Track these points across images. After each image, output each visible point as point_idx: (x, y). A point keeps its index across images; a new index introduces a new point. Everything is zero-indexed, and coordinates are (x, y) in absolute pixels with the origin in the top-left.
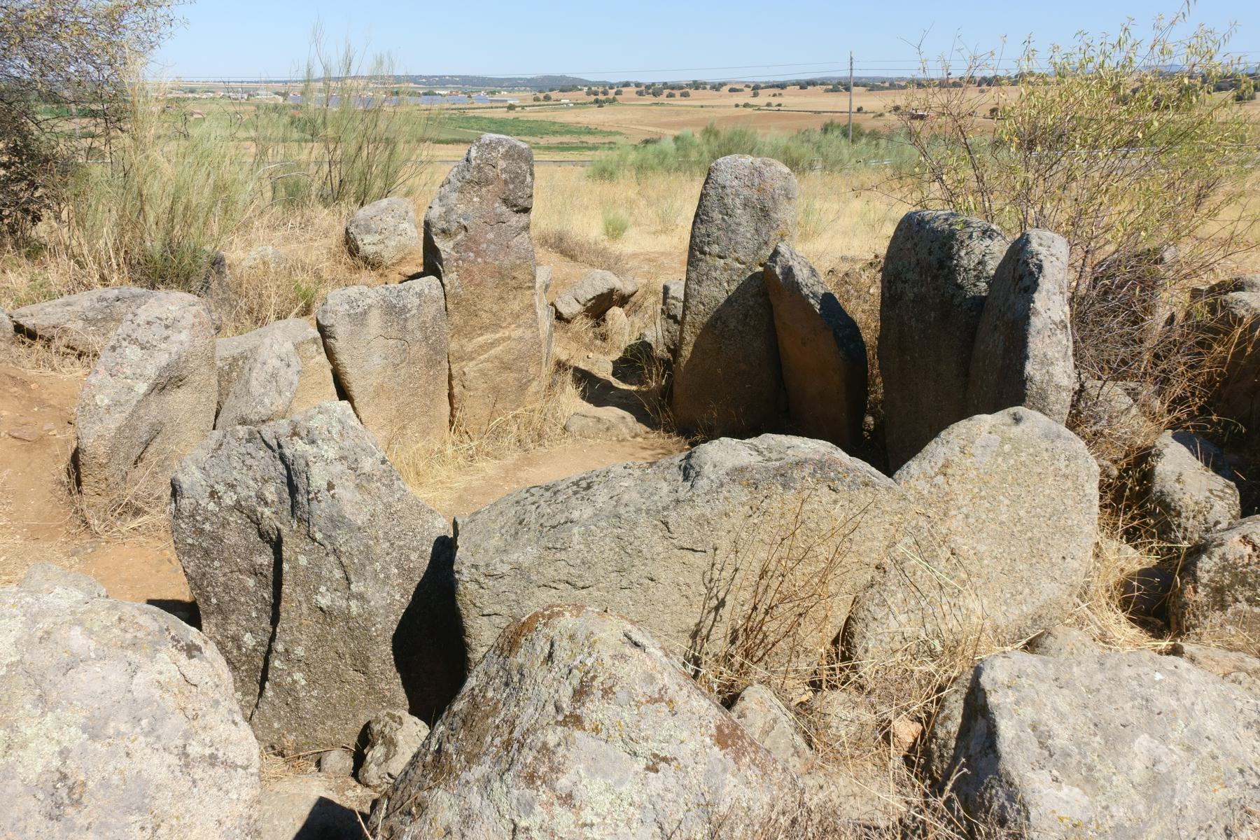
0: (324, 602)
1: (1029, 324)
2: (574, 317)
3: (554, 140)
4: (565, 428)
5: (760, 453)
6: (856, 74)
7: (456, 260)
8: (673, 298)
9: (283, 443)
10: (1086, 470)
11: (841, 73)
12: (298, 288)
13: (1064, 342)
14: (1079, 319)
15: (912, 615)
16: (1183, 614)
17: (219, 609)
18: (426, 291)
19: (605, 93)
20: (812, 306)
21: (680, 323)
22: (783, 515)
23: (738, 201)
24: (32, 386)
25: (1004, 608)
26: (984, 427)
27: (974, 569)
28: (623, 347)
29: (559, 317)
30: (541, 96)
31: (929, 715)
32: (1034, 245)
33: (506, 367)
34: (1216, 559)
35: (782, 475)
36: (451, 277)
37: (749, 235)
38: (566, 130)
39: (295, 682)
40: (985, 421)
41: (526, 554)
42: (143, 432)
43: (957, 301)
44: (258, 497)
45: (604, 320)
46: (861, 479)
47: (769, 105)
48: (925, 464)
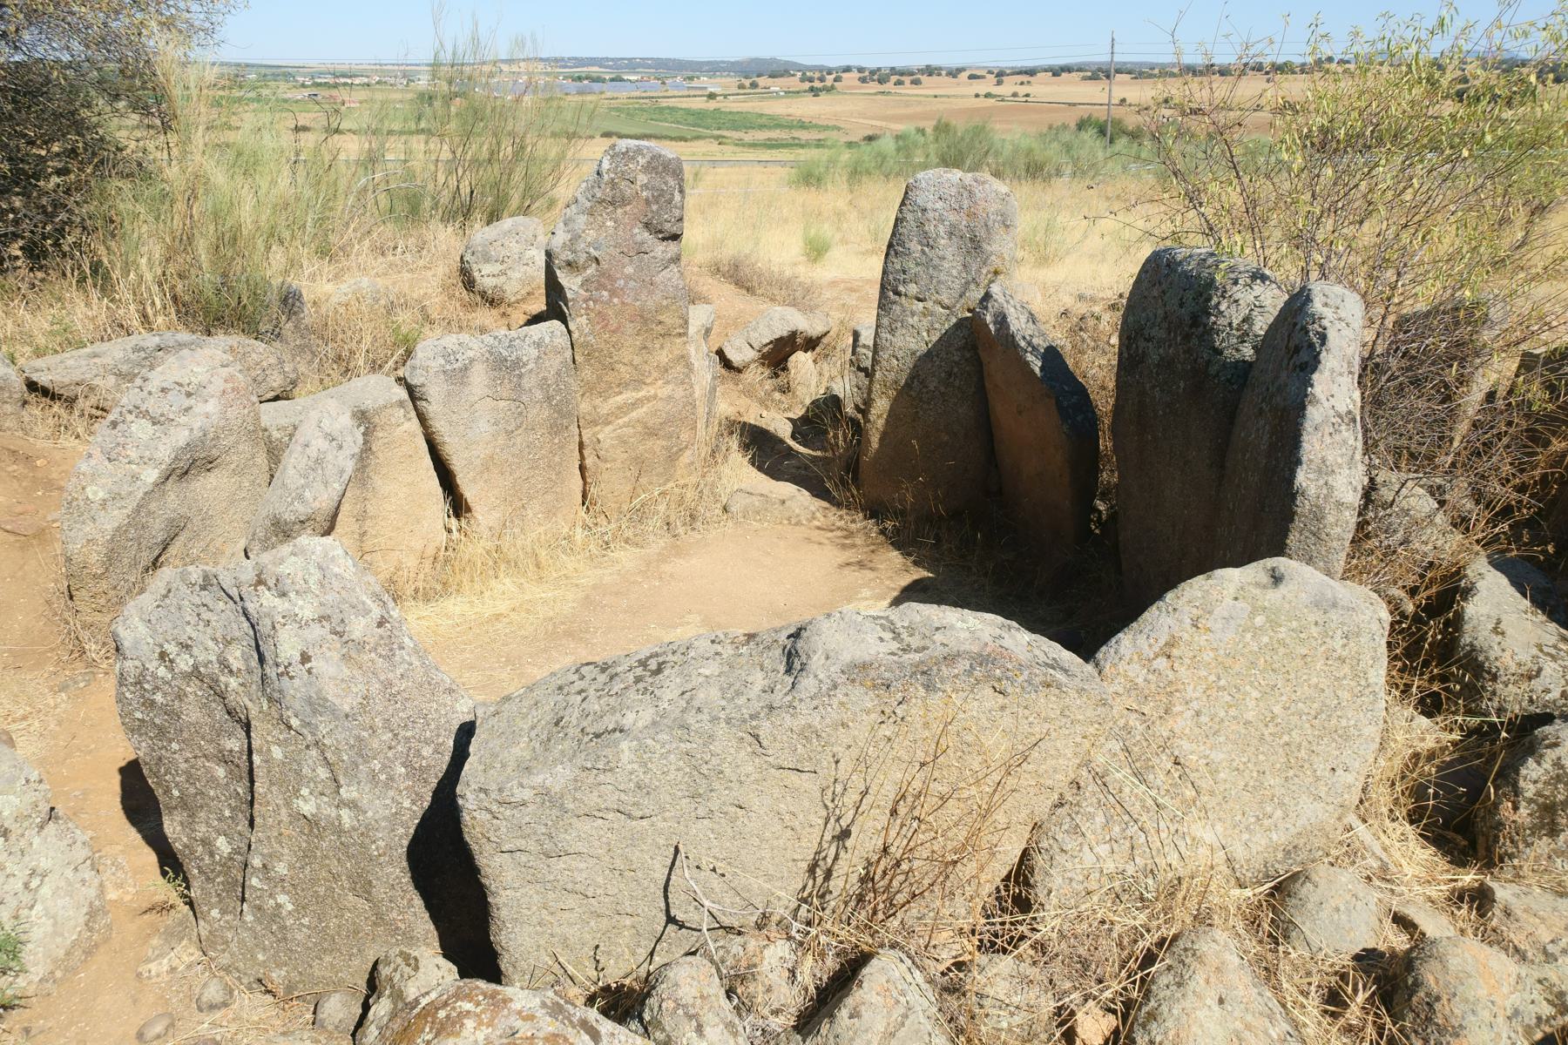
0: (307, 808)
1: (1304, 416)
2: (747, 366)
3: (761, 135)
4: (725, 509)
5: (897, 636)
6: (1117, 58)
7: (586, 301)
8: (864, 346)
9: (244, 590)
10: (1368, 616)
11: (1100, 56)
12: (396, 330)
13: (1351, 442)
14: (1374, 403)
15: (1115, 846)
16: (1496, 838)
17: (184, 803)
18: (547, 340)
19: (822, 80)
20: (1027, 364)
21: (869, 374)
22: (926, 725)
23: (941, 229)
24: (38, 463)
25: (1246, 836)
26: (1227, 588)
27: (1204, 784)
28: (808, 402)
29: (727, 364)
30: (747, 83)
31: (1129, 1004)
32: (1317, 306)
33: (651, 433)
34: (1547, 765)
35: (924, 673)
36: (579, 322)
37: (954, 272)
38: (776, 123)
39: (278, 906)
40: (1230, 579)
41: (558, 777)
42: (157, 530)
43: (1213, 370)
44: (220, 663)
45: (785, 369)
46: (1041, 678)
47: (1015, 95)
48: (1142, 640)
